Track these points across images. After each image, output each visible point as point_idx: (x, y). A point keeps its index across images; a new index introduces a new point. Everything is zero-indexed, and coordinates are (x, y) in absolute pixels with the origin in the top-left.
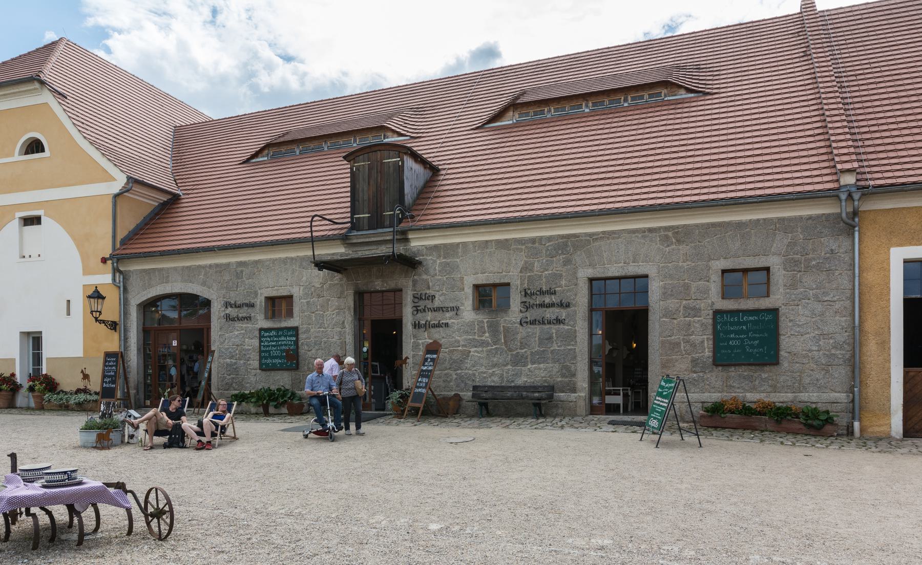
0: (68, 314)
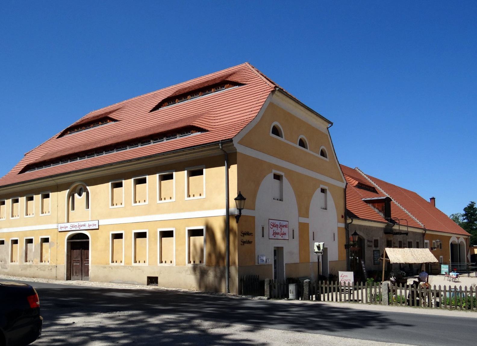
0: (334, 240)
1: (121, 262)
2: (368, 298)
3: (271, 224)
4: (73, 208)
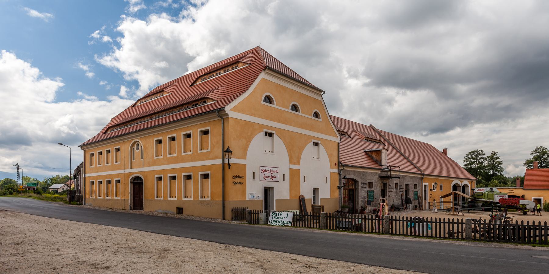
1: (208, 198)
2: (257, 220)
3: (262, 170)
4: (134, 160)
